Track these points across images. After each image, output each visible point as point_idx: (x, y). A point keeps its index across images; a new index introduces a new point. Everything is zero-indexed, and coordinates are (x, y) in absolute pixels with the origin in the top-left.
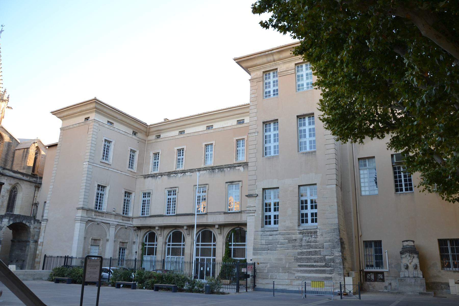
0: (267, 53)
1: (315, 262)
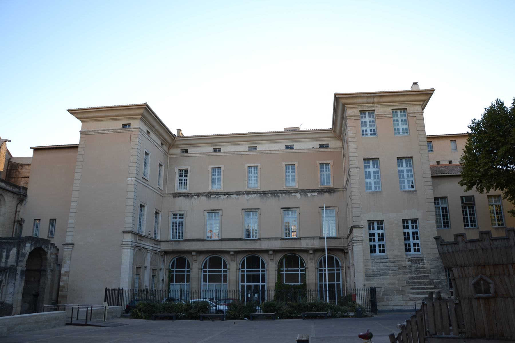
0: (370, 95)
1: (425, 285)
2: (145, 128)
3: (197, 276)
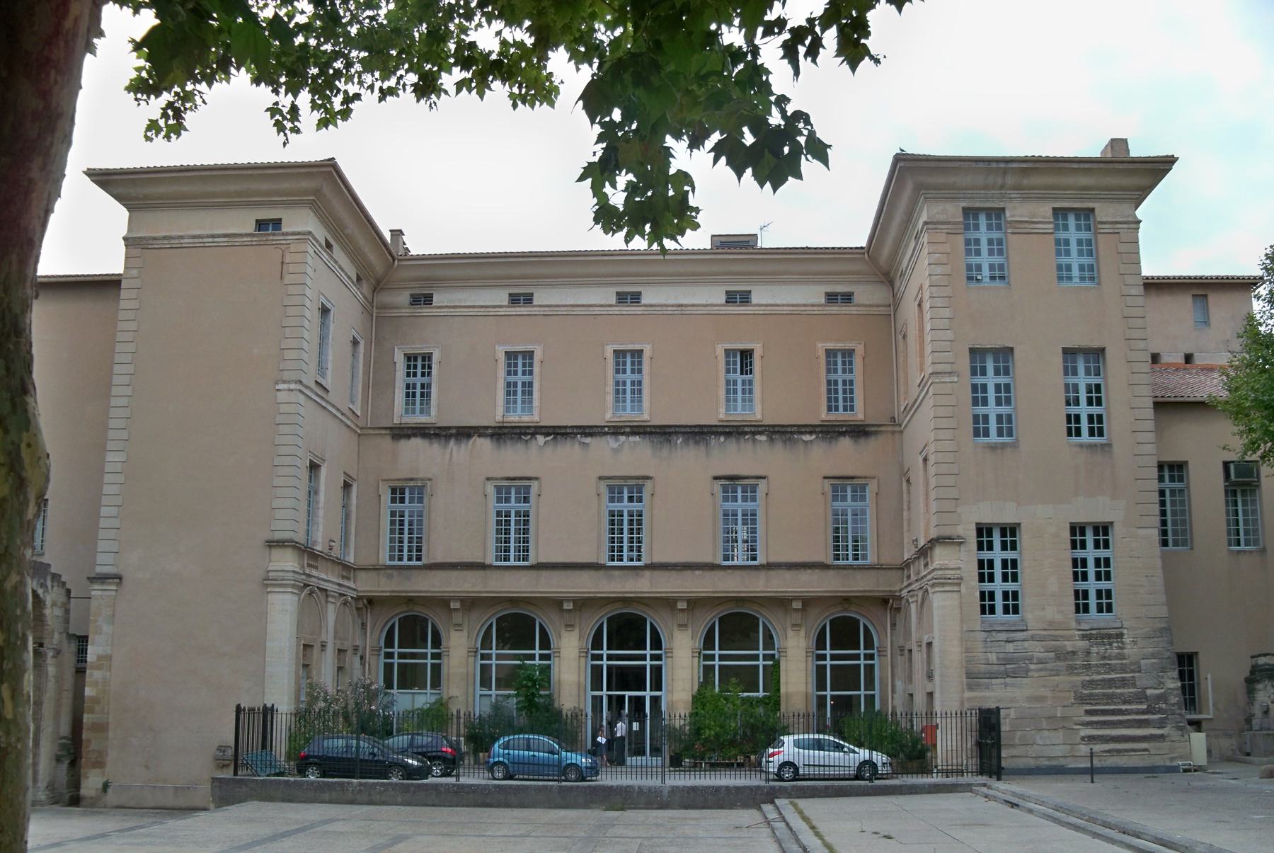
1: (1124, 702)
2: (321, 234)
3: (464, 670)
